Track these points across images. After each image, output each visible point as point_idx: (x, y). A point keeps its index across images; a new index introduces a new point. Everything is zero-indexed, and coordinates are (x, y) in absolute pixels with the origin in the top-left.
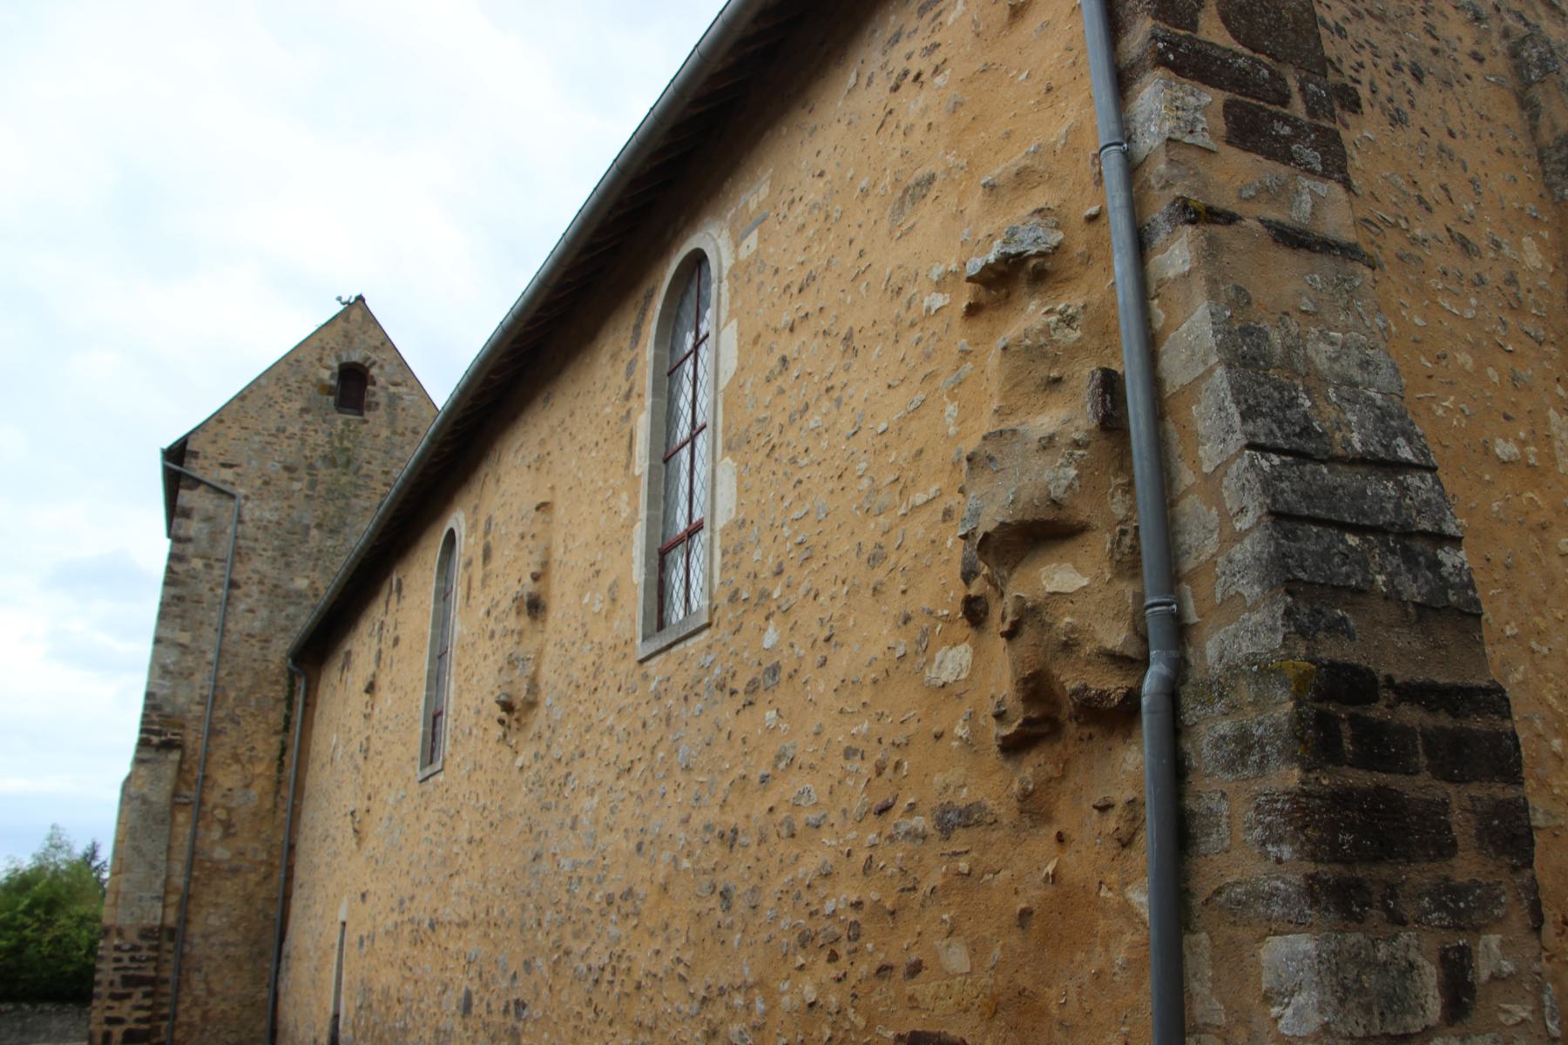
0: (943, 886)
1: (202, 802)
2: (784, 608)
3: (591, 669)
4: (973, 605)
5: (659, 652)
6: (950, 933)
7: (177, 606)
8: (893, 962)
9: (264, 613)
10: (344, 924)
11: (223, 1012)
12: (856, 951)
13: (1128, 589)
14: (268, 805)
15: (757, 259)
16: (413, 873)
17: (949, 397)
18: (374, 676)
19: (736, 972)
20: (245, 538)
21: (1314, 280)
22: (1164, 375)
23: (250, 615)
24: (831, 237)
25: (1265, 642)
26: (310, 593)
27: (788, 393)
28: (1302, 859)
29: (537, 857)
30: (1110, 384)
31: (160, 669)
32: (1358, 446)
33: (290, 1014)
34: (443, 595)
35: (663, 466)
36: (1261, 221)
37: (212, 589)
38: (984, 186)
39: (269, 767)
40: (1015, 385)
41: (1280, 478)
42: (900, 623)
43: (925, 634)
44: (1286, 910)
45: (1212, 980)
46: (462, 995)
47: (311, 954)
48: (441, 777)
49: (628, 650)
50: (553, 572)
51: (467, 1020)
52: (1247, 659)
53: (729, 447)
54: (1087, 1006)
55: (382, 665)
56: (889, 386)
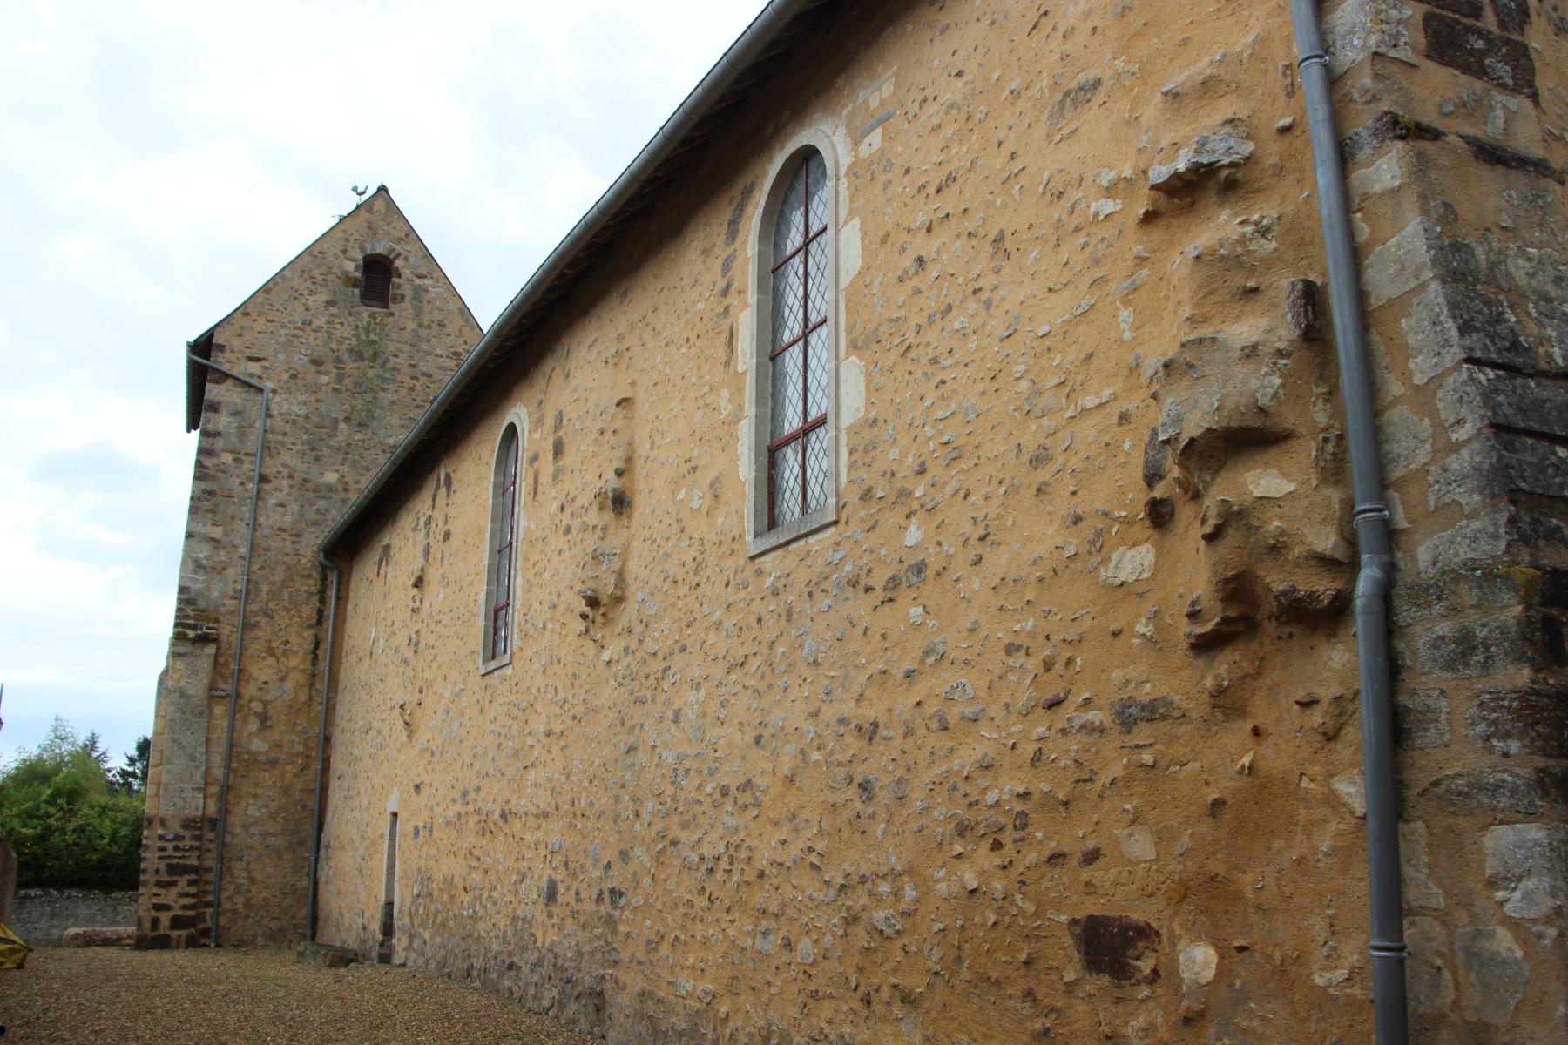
0: (1124, 777)
1: (238, 696)
2: (929, 507)
3: (690, 565)
4: (1159, 507)
5: (774, 549)
6: (1133, 822)
7: (208, 500)
8: (1066, 849)
9: (294, 507)
10: (395, 815)
11: (265, 899)
12: (1023, 839)
13: (1334, 495)
14: (303, 698)
15: (883, 160)
16: (477, 765)
17: (1122, 302)
18: (422, 570)
19: (881, 861)
20: (274, 432)
21: (1511, 196)
22: (1369, 288)
23: (281, 509)
24: (974, 138)
25: (1486, 548)
26: (340, 487)
27: (926, 294)
28: (1532, 753)
29: (631, 750)
30: (1312, 297)
31: (193, 563)
32: (1560, 361)
33: (331, 901)
34: (505, 490)
35: (770, 364)
36: (1462, 137)
37: (242, 484)
38: (1166, 94)
39: (303, 661)
40: (1210, 293)
41: (1496, 391)
42: (1068, 523)
43: (1099, 534)
44: (1514, 801)
45: (1428, 865)
46: (544, 882)
47: (357, 843)
48: (508, 671)
49: (736, 546)
50: (638, 468)
51: (551, 908)
52: (1465, 564)
53: (854, 346)
54: (1287, 891)
55: (431, 560)
56: (1050, 290)
